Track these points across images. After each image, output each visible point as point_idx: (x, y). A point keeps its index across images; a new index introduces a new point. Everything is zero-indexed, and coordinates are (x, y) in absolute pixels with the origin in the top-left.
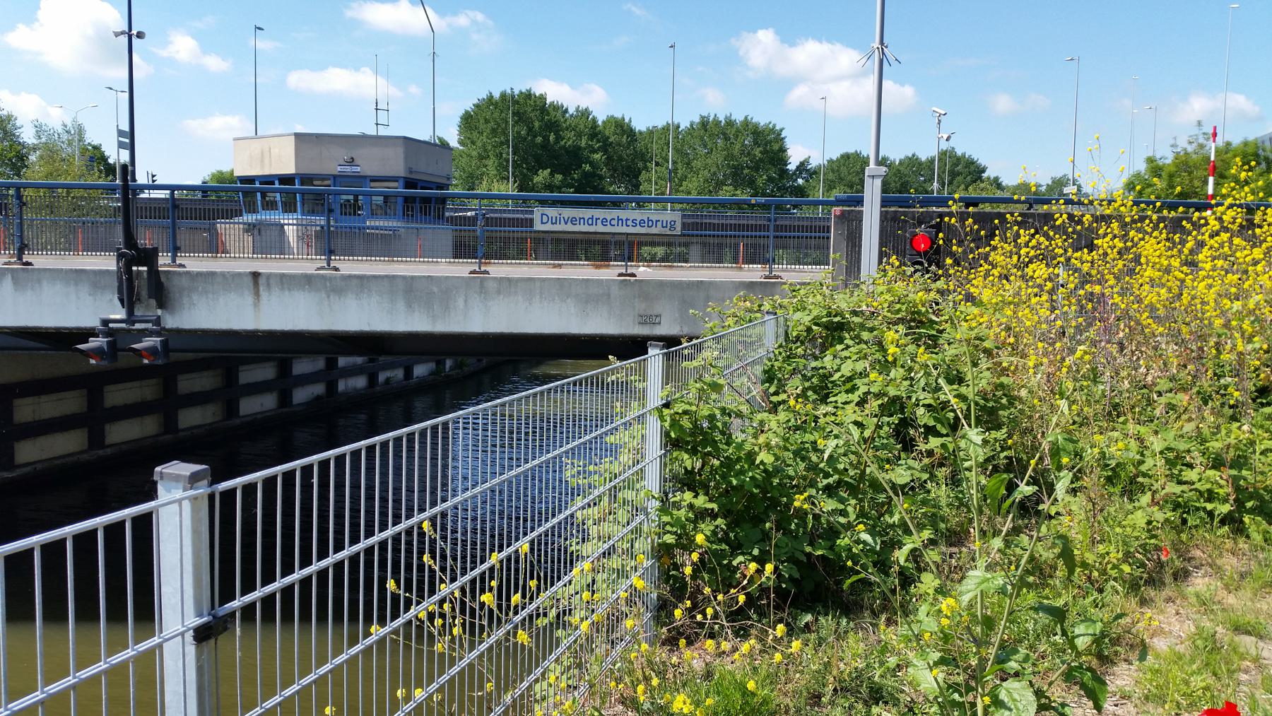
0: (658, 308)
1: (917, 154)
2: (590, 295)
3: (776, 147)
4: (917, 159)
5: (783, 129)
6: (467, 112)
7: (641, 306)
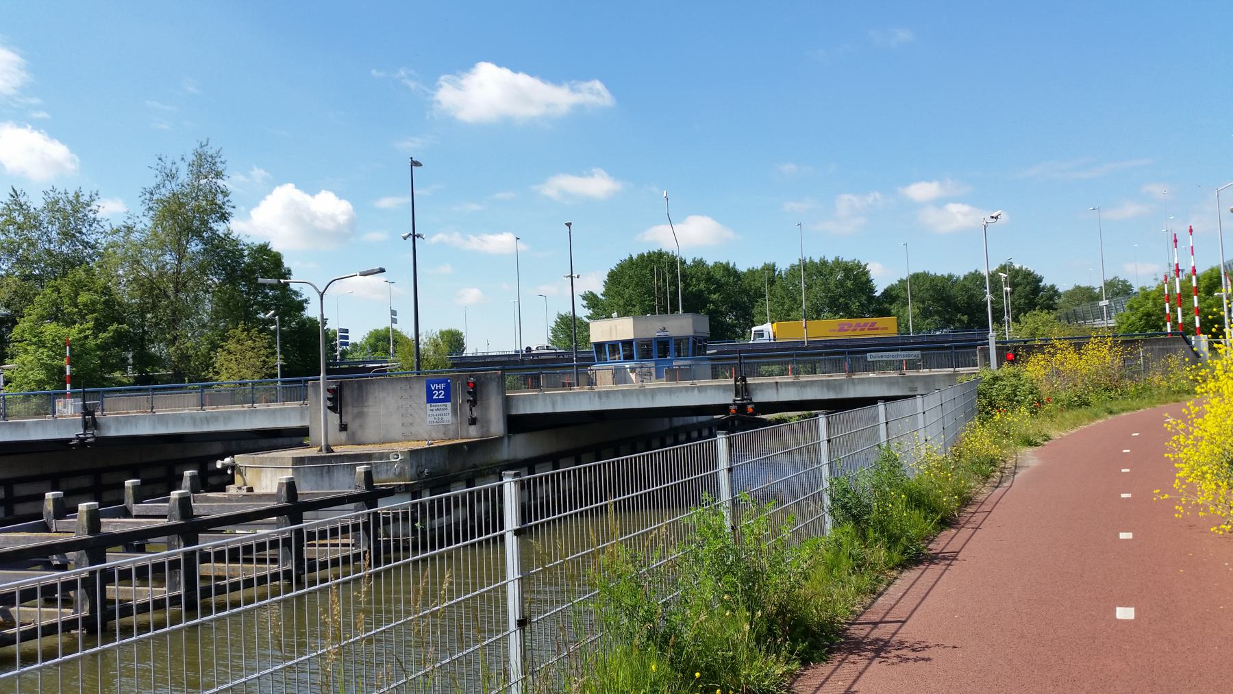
0: (916, 385)
1: (979, 270)
2: (891, 382)
4: (979, 274)
5: (867, 264)
6: (612, 271)
7: (910, 385)
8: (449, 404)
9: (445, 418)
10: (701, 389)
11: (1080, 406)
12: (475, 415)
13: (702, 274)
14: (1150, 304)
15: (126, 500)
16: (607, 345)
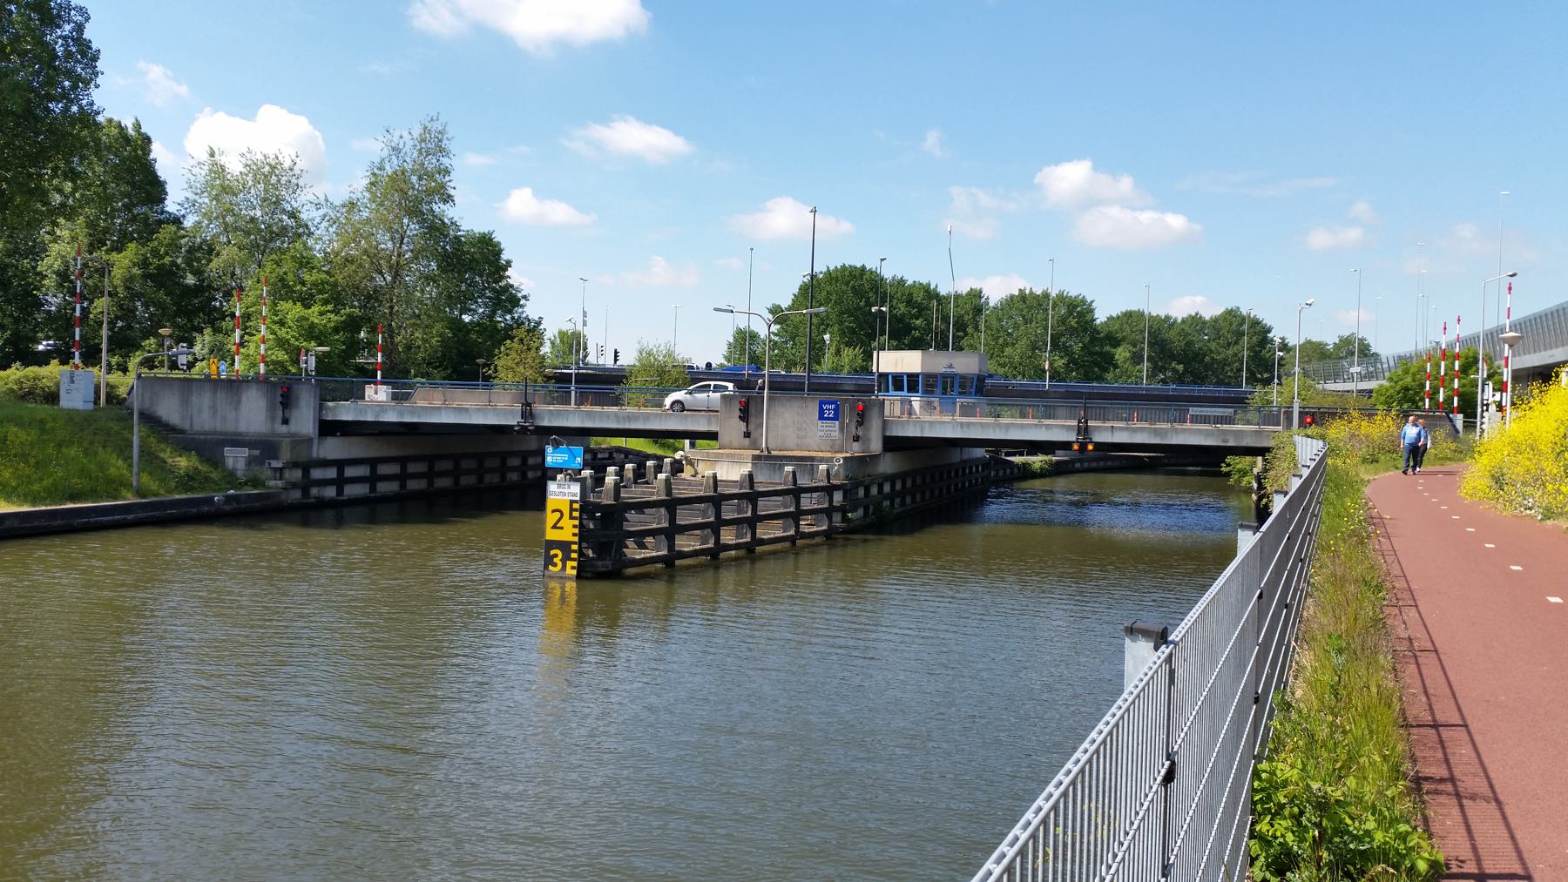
1: (1200, 312)
3: (115, 131)
4: (1201, 317)
7: (1223, 437)
8: (837, 422)
9: (833, 434)
10: (1048, 427)
11: (1372, 462)
12: (860, 434)
13: (902, 295)
14: (1409, 379)
15: (648, 476)
16: (890, 377)
